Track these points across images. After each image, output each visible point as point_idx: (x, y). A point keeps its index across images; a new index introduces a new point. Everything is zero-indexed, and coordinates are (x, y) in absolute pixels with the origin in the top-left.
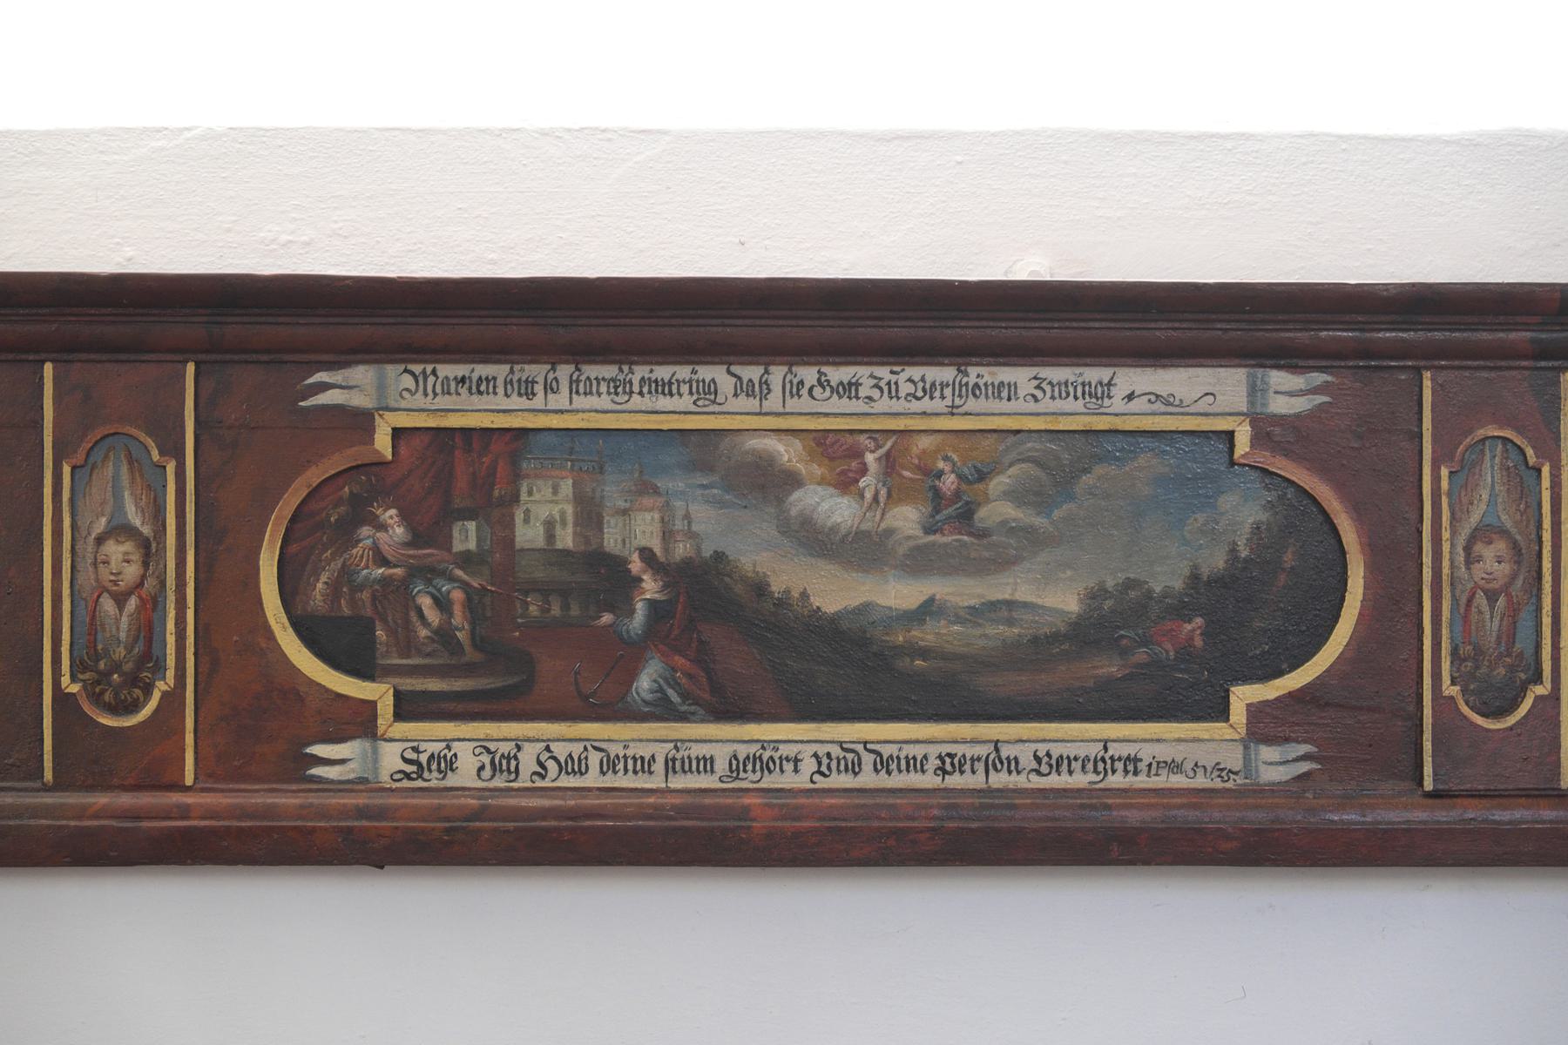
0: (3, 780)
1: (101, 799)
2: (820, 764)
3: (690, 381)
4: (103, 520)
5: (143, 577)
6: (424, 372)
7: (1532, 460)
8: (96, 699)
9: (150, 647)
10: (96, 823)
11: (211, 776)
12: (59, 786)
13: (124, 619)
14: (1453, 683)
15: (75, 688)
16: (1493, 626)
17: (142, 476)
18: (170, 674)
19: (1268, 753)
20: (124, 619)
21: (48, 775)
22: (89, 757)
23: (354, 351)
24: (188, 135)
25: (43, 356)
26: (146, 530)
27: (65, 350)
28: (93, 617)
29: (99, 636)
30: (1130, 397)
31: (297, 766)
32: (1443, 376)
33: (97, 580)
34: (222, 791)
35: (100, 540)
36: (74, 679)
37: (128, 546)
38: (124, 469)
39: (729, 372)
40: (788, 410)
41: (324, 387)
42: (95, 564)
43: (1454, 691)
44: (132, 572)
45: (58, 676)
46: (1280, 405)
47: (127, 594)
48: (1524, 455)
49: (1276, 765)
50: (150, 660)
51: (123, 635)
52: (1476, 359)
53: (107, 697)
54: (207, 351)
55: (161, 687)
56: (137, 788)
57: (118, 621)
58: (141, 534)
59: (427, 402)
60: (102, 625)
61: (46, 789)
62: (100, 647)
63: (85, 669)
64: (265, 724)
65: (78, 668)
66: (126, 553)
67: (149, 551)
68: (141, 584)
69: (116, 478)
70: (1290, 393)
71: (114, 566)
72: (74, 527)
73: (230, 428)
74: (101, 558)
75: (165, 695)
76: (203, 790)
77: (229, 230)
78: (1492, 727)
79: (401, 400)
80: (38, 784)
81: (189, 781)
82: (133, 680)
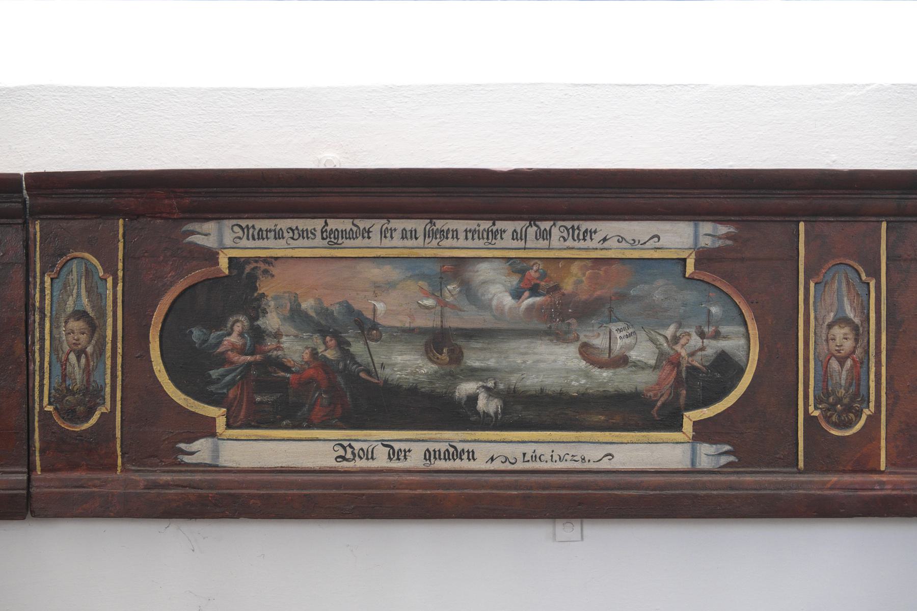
0: (2, 466)
1: (834, 478)
2: (405, 455)
3: (275, 230)
4: (832, 314)
5: (855, 348)
6: (573, 227)
7: (864, 277)
8: (828, 419)
9: (859, 389)
10: (831, 492)
11: (893, 465)
12: (808, 470)
13: (844, 373)
14: (50, 404)
15: (816, 413)
16: (78, 374)
17: (854, 289)
18: (872, 405)
19: (706, 449)
20: (844, 373)
21: (801, 464)
22: (825, 453)
23: (708, 214)
24: (868, 88)
25: (799, 219)
26: (857, 320)
27: (812, 214)
28: (826, 372)
29: (830, 383)
30: (605, 240)
31: (170, 456)
32: (45, 223)
33: (828, 350)
34: (902, 474)
35: (830, 326)
36: (816, 408)
37: (846, 330)
38: (844, 285)
39: (353, 224)
40: (383, 246)
41: (193, 233)
42: (827, 340)
43: (49, 408)
44: (848, 345)
45: (44, 403)
46: (706, 242)
47: (847, 358)
48: (859, 275)
49: (709, 456)
50: (859, 397)
51: (843, 382)
52: (58, 214)
53: (834, 418)
54: (894, 215)
55: (867, 412)
56: (854, 471)
57: (840, 374)
58: (854, 322)
59: (251, 243)
60: (831, 376)
61: (800, 472)
62: (830, 389)
63: (821, 402)
64: (156, 432)
65: (818, 401)
66: (846, 334)
67: (859, 332)
68: (854, 352)
69: (839, 290)
70: (711, 234)
71: (838, 342)
72: (816, 318)
73: (905, 260)
74: (830, 337)
75: (869, 417)
76: (890, 473)
77: (891, 144)
78: (847, 434)
79: (225, 240)
80: (795, 470)
81: (883, 468)
82: (848, 409)
